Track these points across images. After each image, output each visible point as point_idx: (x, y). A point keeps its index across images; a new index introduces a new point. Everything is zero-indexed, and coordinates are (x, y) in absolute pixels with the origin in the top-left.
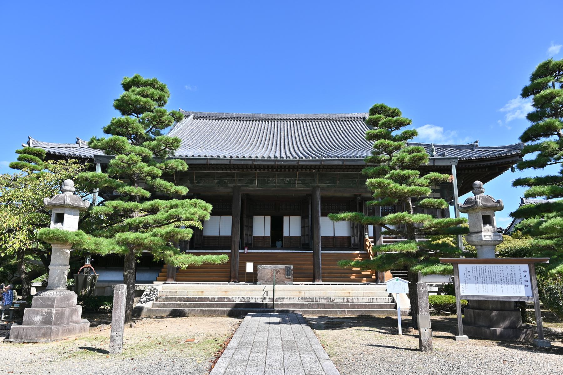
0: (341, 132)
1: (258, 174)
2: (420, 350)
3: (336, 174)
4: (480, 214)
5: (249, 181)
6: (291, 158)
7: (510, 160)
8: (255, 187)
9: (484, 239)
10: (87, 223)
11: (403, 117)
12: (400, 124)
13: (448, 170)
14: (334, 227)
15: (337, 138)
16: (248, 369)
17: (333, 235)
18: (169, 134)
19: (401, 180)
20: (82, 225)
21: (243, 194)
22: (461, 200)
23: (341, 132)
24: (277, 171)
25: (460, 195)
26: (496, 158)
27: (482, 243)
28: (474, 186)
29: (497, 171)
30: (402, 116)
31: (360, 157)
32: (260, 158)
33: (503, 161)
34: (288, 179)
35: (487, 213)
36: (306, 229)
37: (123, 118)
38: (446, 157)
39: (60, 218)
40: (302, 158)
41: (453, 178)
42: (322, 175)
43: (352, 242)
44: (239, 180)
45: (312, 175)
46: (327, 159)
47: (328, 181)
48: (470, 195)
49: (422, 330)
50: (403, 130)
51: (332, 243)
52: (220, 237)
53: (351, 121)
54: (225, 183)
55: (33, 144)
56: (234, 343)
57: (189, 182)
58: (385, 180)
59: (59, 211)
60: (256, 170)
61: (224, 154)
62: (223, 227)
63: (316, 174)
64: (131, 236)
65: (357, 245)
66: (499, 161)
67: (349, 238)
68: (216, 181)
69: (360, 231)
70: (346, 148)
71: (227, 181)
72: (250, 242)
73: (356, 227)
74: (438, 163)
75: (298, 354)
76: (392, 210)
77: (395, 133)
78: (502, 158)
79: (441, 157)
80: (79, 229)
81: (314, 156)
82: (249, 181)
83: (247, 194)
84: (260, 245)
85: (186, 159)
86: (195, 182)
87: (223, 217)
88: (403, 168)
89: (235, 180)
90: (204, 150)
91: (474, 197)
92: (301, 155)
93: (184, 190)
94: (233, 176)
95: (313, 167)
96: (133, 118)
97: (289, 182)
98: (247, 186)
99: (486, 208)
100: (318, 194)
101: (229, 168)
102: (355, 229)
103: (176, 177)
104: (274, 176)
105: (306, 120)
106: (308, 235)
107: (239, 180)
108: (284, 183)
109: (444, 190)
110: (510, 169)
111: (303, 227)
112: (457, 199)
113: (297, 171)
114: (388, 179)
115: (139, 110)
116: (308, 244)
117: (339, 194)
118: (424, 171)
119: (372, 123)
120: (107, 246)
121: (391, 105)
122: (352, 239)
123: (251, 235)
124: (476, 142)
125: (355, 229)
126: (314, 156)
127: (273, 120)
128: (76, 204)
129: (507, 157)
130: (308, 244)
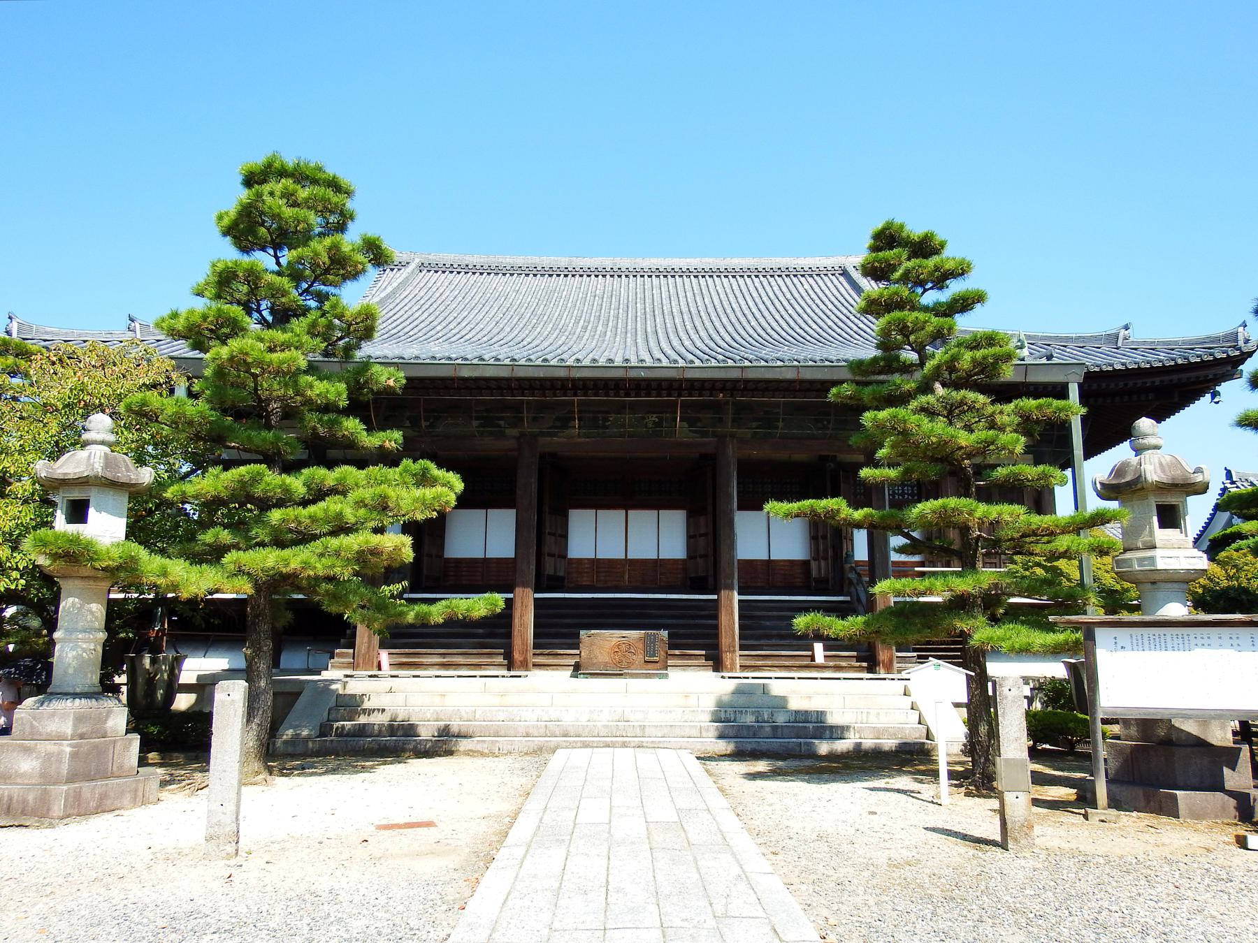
0: (785, 303)
1: (580, 403)
2: (1003, 845)
3: (777, 404)
4: (1152, 502)
5: (558, 424)
6: (665, 363)
7: (1210, 373)
8: (573, 438)
9: (1161, 565)
10: (151, 521)
11: (951, 254)
12: (941, 278)
13: (1060, 391)
14: (771, 533)
15: (778, 317)
16: (561, 903)
17: (766, 558)
18: (352, 297)
19: (952, 412)
20: (135, 531)
21: (542, 456)
22: (1099, 468)
23: (785, 303)
24: (627, 395)
25: (1088, 454)
26: (1177, 368)
27: (1157, 577)
28: (1134, 432)
29: (1176, 400)
30: (947, 253)
31: (838, 360)
32: (586, 362)
33: (1193, 375)
34: (654, 418)
35: (1171, 500)
36: (702, 541)
37: (246, 260)
38: (1055, 361)
39: (78, 512)
40: (692, 362)
41: (1074, 408)
42: (740, 408)
43: (814, 574)
44: (535, 419)
45: (717, 407)
46: (755, 364)
47: (754, 424)
48: (1121, 453)
49: (1009, 797)
50: (955, 287)
51: (762, 575)
52: (486, 561)
53: (811, 276)
54: (499, 426)
55: (19, 332)
56: (523, 830)
57: (408, 424)
58: (907, 414)
59: (76, 495)
60: (575, 395)
61: (494, 354)
62: (491, 535)
63: (727, 403)
64: (269, 559)
65: (826, 581)
66: (1184, 376)
67: (805, 564)
68: (475, 423)
69: (833, 547)
70: (801, 341)
71: (502, 423)
72: (561, 574)
73: (825, 537)
74: (1034, 377)
75: (691, 858)
76: (912, 495)
77: (931, 297)
78: (1190, 367)
79: (1044, 361)
80: (127, 537)
81: (720, 357)
82: (558, 424)
83: (553, 455)
84: (585, 581)
85: (399, 364)
86: (424, 424)
87: (494, 513)
88: (957, 386)
89: (522, 419)
90: (446, 345)
91: (1134, 460)
92: (691, 357)
93: (392, 439)
94: (517, 407)
95: (718, 385)
96: (264, 260)
97: (658, 425)
98: (554, 435)
99: (1161, 488)
100: (732, 455)
101: (510, 388)
102: (821, 541)
103: (374, 406)
104: (621, 408)
105: (698, 274)
106: (704, 556)
107: (535, 419)
108: (646, 426)
109: (1050, 444)
110: (1208, 396)
111: (691, 537)
112: (1081, 467)
113: (680, 395)
114: (915, 412)
115: (283, 238)
116: (705, 579)
117: (783, 455)
118: (1004, 393)
119: (876, 272)
120: (192, 580)
121: (915, 229)
122: (814, 565)
123: (564, 556)
124: (1126, 328)
125: (821, 541)
126: (720, 357)
127: (616, 273)
128: (122, 476)
129: (1203, 365)
130: (705, 579)
